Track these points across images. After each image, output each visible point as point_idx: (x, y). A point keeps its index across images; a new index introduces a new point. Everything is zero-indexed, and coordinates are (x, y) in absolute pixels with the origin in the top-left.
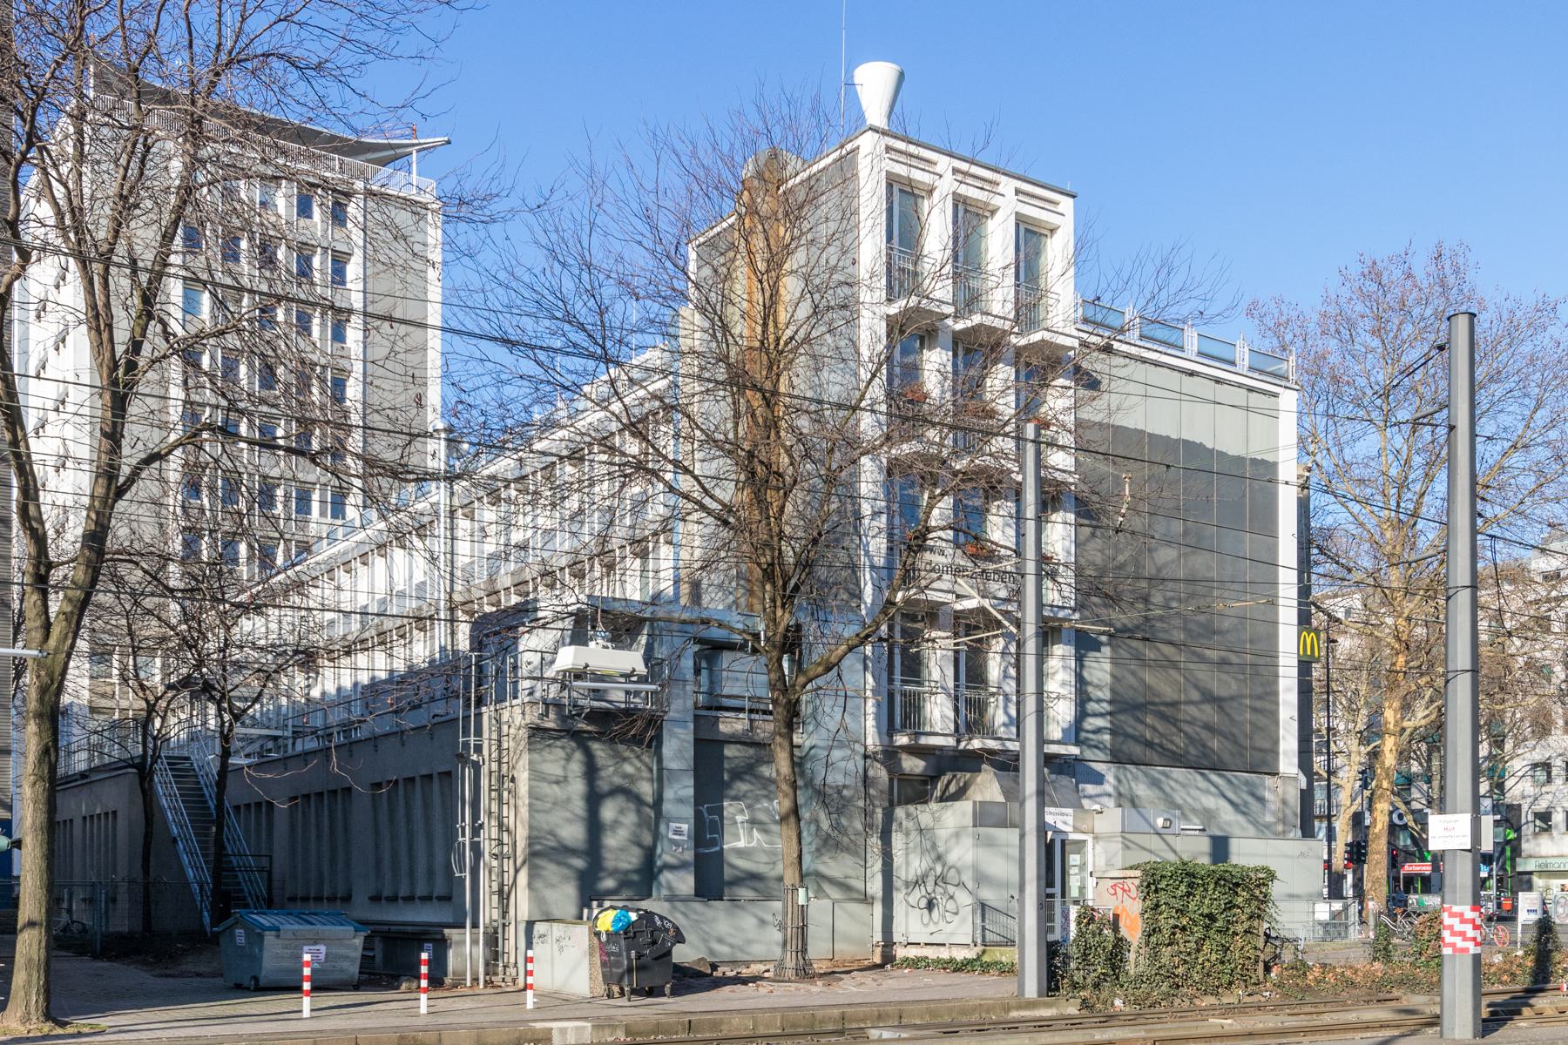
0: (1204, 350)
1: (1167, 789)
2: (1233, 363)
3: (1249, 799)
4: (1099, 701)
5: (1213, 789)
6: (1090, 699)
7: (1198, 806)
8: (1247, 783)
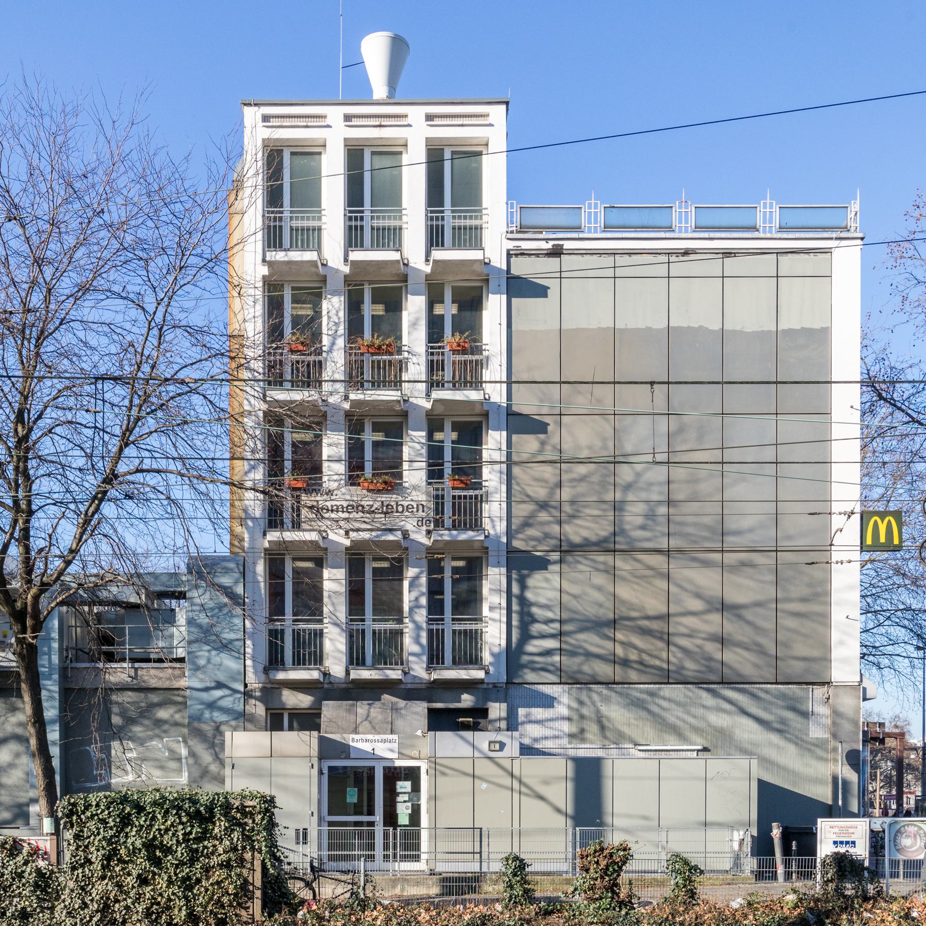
0: (703, 223)
1: (655, 709)
2: (755, 228)
3: (790, 715)
4: (548, 621)
5: (727, 706)
6: (535, 621)
7: (702, 724)
8: (783, 696)
